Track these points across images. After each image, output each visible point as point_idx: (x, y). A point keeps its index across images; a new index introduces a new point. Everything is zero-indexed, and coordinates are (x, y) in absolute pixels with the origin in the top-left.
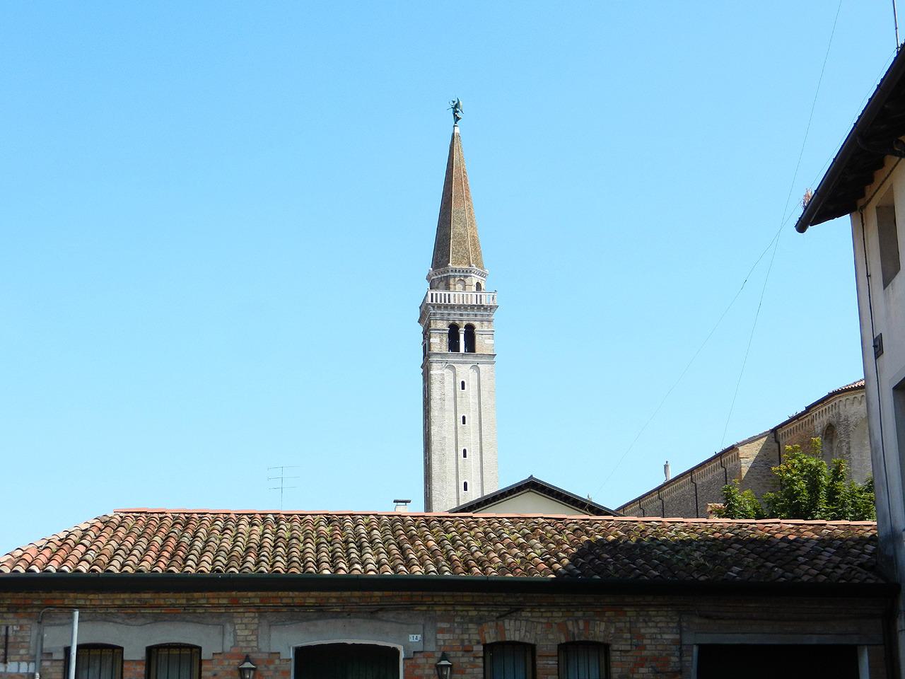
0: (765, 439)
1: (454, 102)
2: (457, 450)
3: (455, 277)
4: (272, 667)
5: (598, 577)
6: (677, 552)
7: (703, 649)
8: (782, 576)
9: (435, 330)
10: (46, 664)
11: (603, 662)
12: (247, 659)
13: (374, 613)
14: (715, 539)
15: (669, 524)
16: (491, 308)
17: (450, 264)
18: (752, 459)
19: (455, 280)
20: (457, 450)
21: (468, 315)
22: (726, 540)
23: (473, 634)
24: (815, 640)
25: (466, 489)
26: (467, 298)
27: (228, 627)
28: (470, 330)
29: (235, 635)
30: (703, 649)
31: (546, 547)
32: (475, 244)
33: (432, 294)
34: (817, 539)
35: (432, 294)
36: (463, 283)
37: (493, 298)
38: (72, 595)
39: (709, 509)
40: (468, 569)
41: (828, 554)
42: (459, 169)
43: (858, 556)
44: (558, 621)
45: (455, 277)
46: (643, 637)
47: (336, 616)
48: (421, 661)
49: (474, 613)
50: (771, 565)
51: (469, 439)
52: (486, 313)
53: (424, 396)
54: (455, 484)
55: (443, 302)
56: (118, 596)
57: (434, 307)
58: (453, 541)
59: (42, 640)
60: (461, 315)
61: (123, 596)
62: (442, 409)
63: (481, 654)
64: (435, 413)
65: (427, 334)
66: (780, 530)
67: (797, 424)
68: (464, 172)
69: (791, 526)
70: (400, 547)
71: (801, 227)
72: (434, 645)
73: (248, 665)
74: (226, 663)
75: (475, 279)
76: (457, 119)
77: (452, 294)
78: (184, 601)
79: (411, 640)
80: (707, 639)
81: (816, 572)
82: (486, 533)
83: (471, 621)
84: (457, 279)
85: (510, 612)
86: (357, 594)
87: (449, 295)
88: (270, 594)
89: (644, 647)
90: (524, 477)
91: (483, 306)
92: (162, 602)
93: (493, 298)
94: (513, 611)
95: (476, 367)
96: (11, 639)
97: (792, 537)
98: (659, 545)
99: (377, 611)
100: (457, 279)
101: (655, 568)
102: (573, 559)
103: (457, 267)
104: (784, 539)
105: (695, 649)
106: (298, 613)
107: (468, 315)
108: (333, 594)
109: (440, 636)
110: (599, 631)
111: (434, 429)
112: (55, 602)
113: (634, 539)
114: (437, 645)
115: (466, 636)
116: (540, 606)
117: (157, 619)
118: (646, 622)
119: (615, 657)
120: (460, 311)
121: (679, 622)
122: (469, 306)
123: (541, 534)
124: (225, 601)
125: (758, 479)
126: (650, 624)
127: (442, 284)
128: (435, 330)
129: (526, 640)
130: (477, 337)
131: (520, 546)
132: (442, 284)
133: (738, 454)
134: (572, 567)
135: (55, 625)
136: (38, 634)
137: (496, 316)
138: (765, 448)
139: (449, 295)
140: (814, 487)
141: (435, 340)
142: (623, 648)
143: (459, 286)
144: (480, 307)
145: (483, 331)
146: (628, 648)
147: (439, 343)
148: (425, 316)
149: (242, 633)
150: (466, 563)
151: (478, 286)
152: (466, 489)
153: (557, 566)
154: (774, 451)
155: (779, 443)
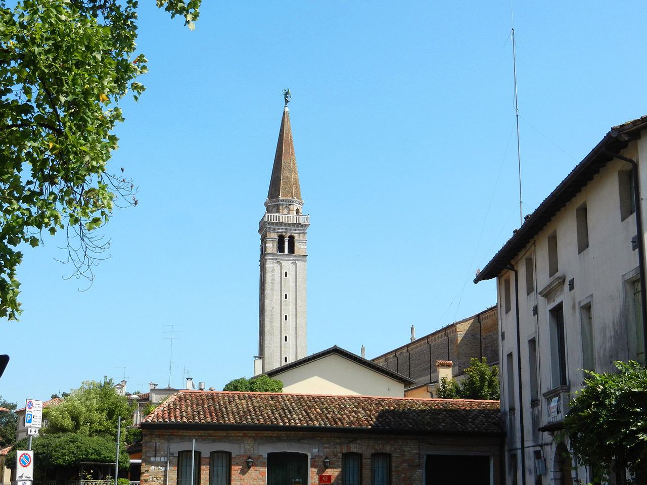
0: (472, 321)
1: (285, 90)
2: (281, 316)
3: (283, 205)
4: (259, 461)
5: (388, 428)
6: (419, 416)
7: (428, 456)
8: (461, 428)
9: (269, 238)
10: (171, 458)
11: (388, 461)
12: (249, 457)
13: (299, 440)
14: (435, 409)
15: (416, 401)
16: (306, 226)
17: (280, 197)
18: (465, 332)
19: (283, 207)
20: (281, 316)
21: (291, 230)
22: (440, 410)
23: (338, 449)
24: (472, 454)
25: (286, 340)
26: (290, 219)
27: (242, 444)
28: (292, 240)
29: (245, 448)
30: (428, 456)
31: (365, 412)
32: (296, 184)
33: (268, 216)
34: (479, 410)
35: (268, 216)
36: (288, 209)
37: (307, 219)
38: (182, 431)
39: (437, 364)
40: (336, 423)
41: (481, 417)
42: (287, 134)
43: (494, 418)
44: (372, 444)
45: (283, 205)
46: (405, 451)
47: (285, 441)
48: (317, 459)
49: (339, 441)
50: (457, 422)
51: (289, 310)
52: (302, 229)
53: (261, 280)
54: (279, 337)
55: (275, 221)
56: (199, 432)
57: (269, 224)
58: (327, 409)
59: (170, 448)
60: (286, 229)
61: (201, 432)
62: (272, 289)
63: (341, 457)
64: (268, 292)
65: (264, 240)
66: (463, 405)
67: (492, 313)
68: (291, 137)
69: (468, 403)
70: (306, 412)
71: (476, 281)
72: (322, 453)
73: (250, 460)
74: (241, 459)
75: (296, 206)
76: (287, 102)
77: (281, 216)
78: (225, 434)
79: (314, 451)
80: (430, 453)
81: (474, 426)
82: (339, 405)
83: (337, 444)
84: (284, 206)
85: (353, 441)
86: (293, 432)
87: (279, 216)
88: (259, 432)
89: (405, 455)
90: (329, 346)
91: (300, 224)
92: (217, 434)
93: (307, 219)
94: (354, 440)
95: (294, 263)
96: (157, 448)
97: (468, 409)
98: (412, 412)
99: (300, 440)
100: (284, 206)
101: (410, 423)
102: (377, 418)
103: (284, 198)
104: (464, 410)
105: (425, 457)
106: (269, 440)
107: (291, 230)
108: (284, 432)
109: (325, 450)
110: (388, 449)
111: (267, 302)
112: (175, 433)
113: (401, 409)
114: (324, 453)
115: (335, 450)
116: (365, 438)
117: (214, 441)
118: (406, 446)
119: (393, 459)
120: (286, 227)
121: (419, 446)
122: (291, 224)
123: (362, 406)
124: (242, 435)
125: (467, 344)
126: (408, 446)
127: (275, 209)
128: (269, 238)
129: (359, 452)
130: (296, 244)
131: (355, 413)
132: (275, 209)
133: (456, 329)
134: (377, 422)
135: (174, 443)
136: (168, 446)
137: (308, 230)
138: (472, 325)
139: (279, 216)
140: (482, 379)
141: (269, 245)
142: (396, 456)
143: (285, 211)
144: (298, 225)
145: (300, 240)
146: (399, 456)
147: (271, 247)
148: (263, 228)
149: (248, 447)
150: (334, 420)
151: (298, 210)
152: (286, 340)
153: (371, 422)
154: (477, 328)
155: (480, 323)
